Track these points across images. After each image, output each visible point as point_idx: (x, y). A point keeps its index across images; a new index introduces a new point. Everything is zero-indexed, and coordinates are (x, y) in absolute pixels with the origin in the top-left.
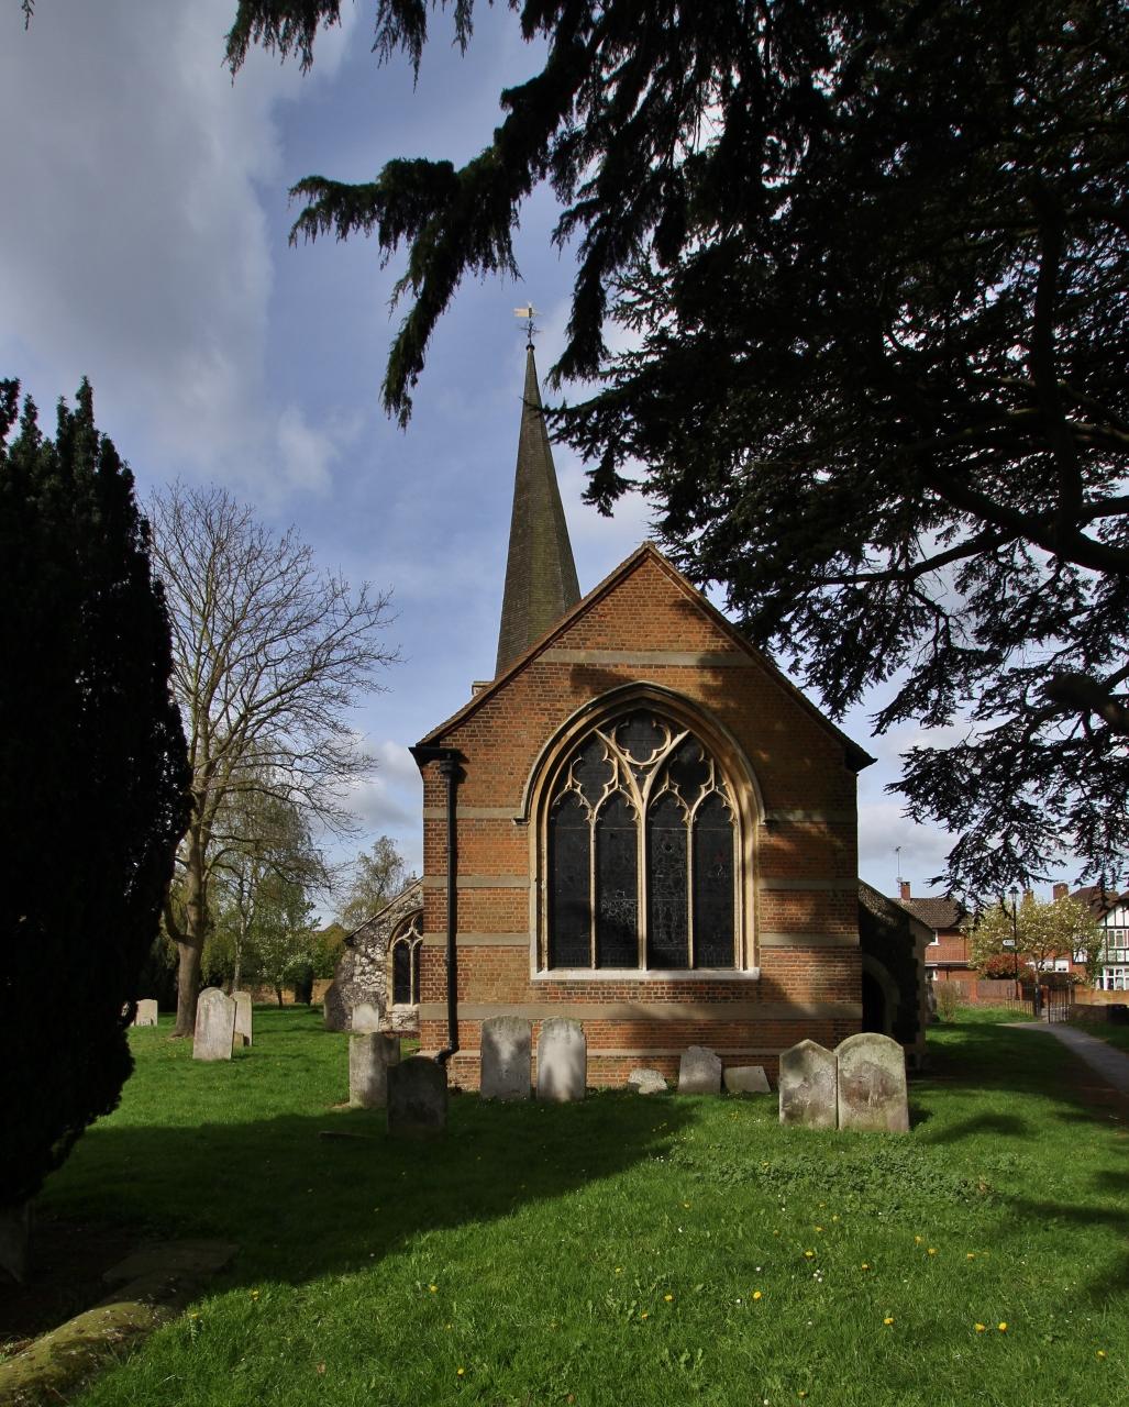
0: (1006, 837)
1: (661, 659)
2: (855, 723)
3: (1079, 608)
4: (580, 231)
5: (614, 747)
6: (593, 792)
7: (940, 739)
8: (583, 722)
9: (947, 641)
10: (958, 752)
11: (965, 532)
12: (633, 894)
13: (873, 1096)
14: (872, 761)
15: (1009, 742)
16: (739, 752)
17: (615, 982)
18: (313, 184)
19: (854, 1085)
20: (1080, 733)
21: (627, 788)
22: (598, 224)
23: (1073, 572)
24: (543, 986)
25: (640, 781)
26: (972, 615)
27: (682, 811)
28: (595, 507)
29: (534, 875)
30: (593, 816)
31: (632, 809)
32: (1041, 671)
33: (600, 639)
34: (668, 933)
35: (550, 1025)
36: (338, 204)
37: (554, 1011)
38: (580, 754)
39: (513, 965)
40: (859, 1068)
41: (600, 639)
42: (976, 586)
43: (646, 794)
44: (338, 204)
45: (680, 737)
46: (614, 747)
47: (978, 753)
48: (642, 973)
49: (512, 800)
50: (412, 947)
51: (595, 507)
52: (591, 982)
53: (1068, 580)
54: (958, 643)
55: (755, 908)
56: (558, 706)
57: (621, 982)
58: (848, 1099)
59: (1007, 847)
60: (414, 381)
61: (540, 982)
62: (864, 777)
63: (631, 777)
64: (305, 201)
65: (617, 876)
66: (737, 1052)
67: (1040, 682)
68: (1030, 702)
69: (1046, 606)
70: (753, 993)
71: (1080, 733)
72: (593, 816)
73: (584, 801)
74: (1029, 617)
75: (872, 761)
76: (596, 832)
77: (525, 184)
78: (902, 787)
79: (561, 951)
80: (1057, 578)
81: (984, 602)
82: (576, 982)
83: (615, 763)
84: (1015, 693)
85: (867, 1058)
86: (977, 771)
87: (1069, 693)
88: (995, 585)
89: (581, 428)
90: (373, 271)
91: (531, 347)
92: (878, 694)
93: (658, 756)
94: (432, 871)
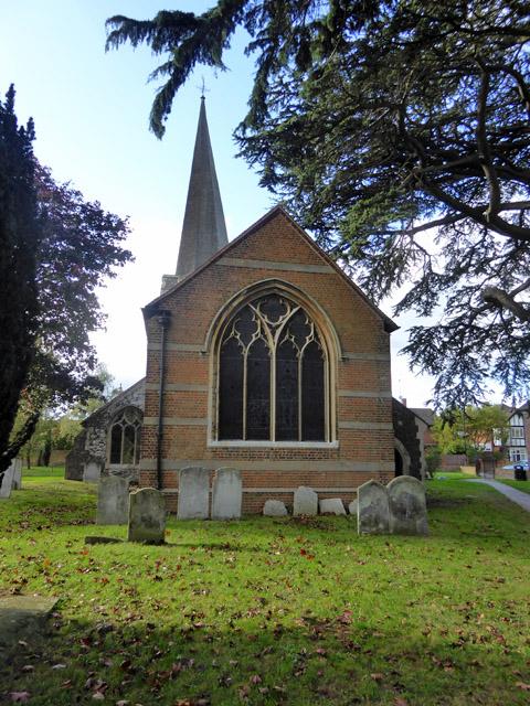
0: (462, 377)
1: (286, 267)
2: (386, 306)
3: (495, 257)
4: (259, 51)
5: (259, 314)
6: (246, 338)
7: (428, 323)
8: (241, 299)
9: (430, 269)
10: (436, 328)
11: (438, 215)
12: (268, 397)
13: (409, 512)
14: (398, 328)
15: (463, 324)
16: (328, 320)
17: (256, 448)
18: (117, 19)
19: (399, 506)
20: (498, 321)
21: (265, 337)
22: (267, 50)
23: (492, 237)
24: (214, 450)
25: (273, 334)
26: (443, 256)
27: (296, 351)
28: (266, 188)
29: (211, 384)
30: (246, 352)
31: (268, 349)
32: (478, 288)
33: (252, 254)
34: (288, 421)
35: (221, 473)
36: (129, 29)
37: (220, 465)
38: (241, 319)
39: (197, 437)
40: (400, 496)
41: (252, 254)
42: (445, 241)
43: (276, 341)
44: (129, 29)
45: (295, 310)
46: (259, 314)
47: (447, 329)
48: (273, 443)
49: (200, 341)
50: (123, 429)
51: (266, 188)
52: (243, 448)
53: (489, 240)
54: (435, 270)
55: (336, 407)
56: (228, 289)
57: (261, 448)
58: (395, 514)
59: (463, 383)
60: (166, 119)
61: (212, 448)
62: (394, 336)
63: (268, 331)
64: (112, 28)
65: (259, 388)
66: (326, 490)
67: (478, 293)
68: (472, 304)
69: (479, 255)
70: (336, 456)
71: (498, 321)
72: (246, 352)
73: (241, 343)
74: (471, 259)
75: (398, 328)
76: (248, 360)
77: (231, 28)
78: (409, 348)
79: (227, 428)
80: (484, 240)
81: (449, 249)
82: (234, 448)
83: (259, 322)
84: (465, 300)
85: (405, 490)
86: (446, 339)
87: (492, 301)
88: (454, 241)
89: (253, 148)
90: (145, 62)
91: (203, 98)
92: (398, 293)
93: (283, 321)
94: (151, 380)
